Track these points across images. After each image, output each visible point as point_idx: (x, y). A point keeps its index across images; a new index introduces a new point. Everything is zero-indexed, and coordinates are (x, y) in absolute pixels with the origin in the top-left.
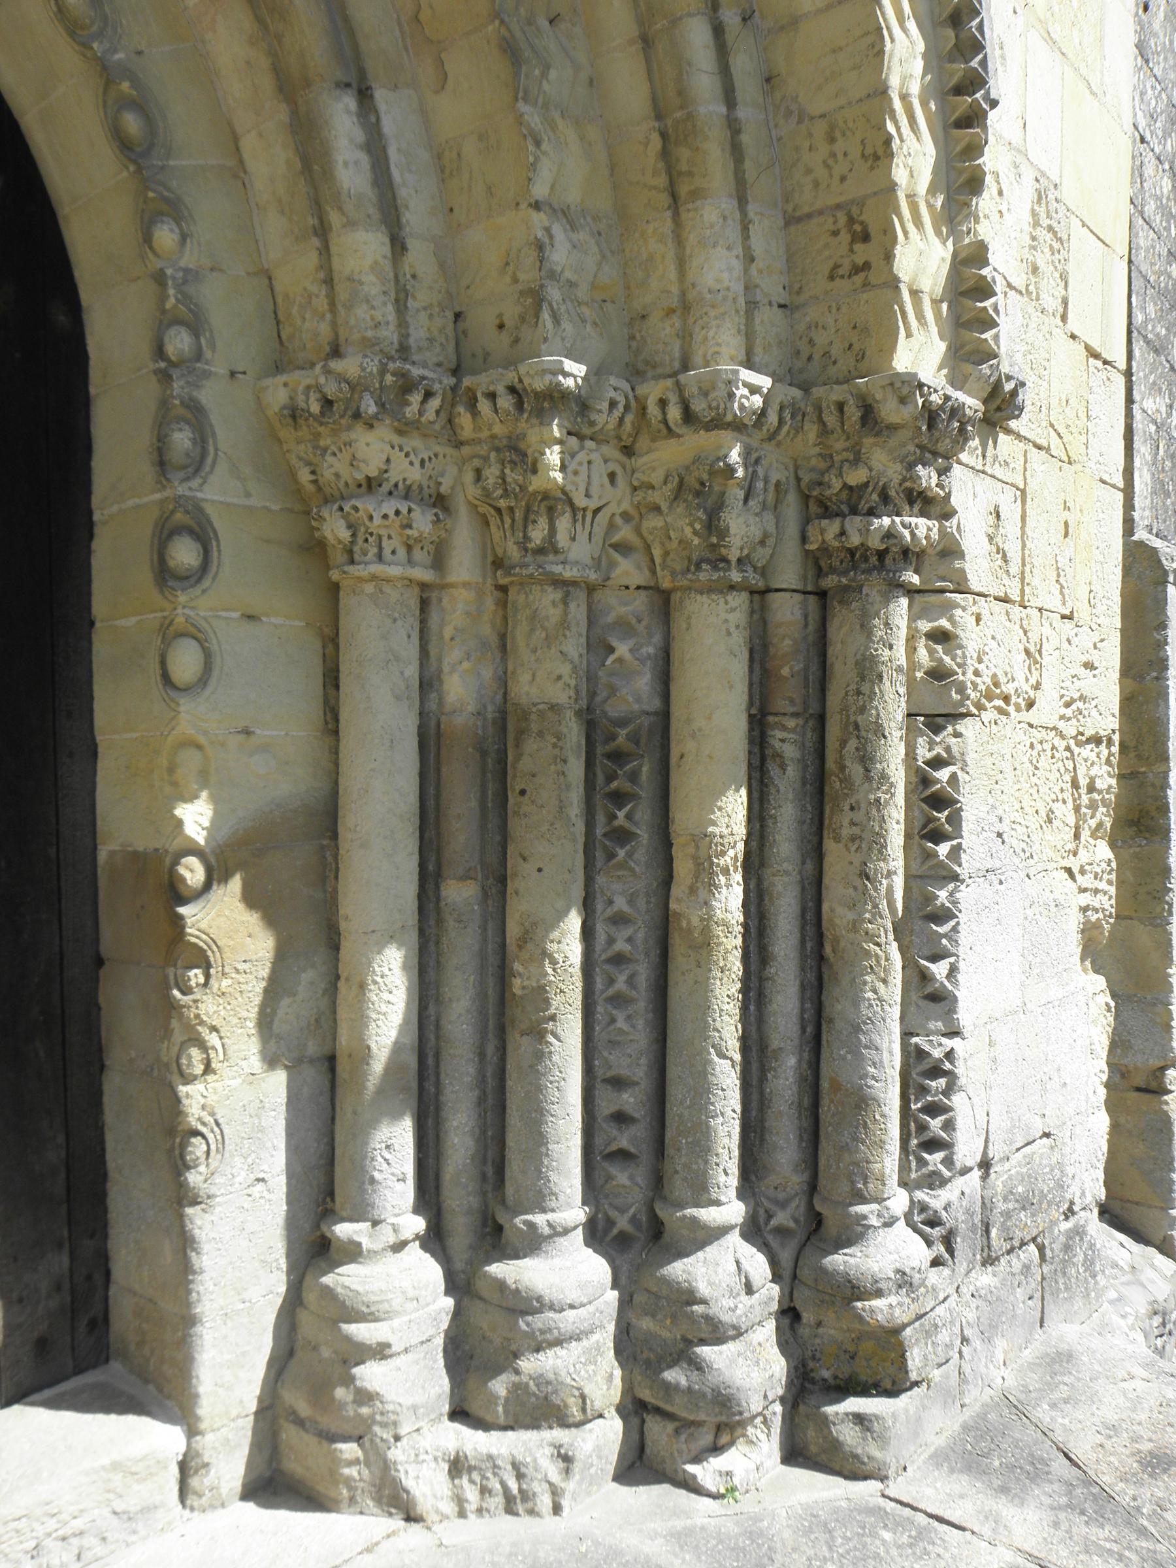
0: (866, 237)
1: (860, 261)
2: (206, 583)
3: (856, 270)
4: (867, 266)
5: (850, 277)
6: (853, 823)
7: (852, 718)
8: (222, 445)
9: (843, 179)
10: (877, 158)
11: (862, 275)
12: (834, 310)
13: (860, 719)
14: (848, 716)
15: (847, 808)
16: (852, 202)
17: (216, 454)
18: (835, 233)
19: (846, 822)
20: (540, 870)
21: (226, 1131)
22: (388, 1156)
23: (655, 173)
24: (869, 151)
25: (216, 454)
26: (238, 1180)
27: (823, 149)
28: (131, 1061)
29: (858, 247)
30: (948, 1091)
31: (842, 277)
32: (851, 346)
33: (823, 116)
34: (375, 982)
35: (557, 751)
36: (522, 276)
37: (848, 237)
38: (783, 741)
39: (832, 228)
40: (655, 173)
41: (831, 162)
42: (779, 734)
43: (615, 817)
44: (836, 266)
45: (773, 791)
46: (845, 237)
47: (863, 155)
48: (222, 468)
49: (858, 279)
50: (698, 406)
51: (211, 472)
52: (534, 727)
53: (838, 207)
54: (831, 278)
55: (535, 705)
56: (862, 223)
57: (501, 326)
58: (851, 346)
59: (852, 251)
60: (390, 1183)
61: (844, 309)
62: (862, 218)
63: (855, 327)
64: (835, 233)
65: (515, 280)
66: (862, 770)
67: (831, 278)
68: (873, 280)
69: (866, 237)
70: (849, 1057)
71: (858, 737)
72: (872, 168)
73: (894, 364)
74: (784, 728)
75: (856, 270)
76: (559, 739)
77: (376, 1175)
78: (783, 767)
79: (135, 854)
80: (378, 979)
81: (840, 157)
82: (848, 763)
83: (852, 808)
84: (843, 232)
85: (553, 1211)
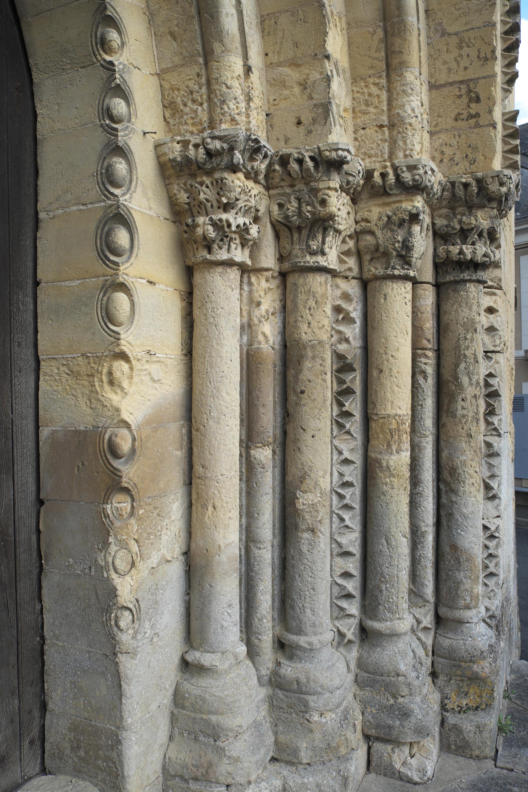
0: (478, 100)
1: (473, 112)
2: (132, 260)
3: (471, 116)
4: (477, 115)
5: (467, 120)
6: (463, 408)
7: (462, 352)
8: (139, 175)
9: (466, 68)
10: (486, 59)
11: (474, 120)
12: (457, 137)
13: (466, 352)
14: (460, 351)
15: (460, 400)
16: (471, 80)
17: (137, 181)
18: (460, 97)
19: (459, 407)
20: (313, 437)
21: (141, 605)
22: (230, 611)
23: (378, 50)
24: (482, 55)
25: (137, 181)
26: (147, 635)
27: (455, 53)
28: (69, 566)
29: (473, 105)
30: (497, 546)
31: (463, 119)
32: (467, 156)
33: (456, 34)
34: (222, 506)
35: (322, 368)
36: (315, 96)
37: (467, 100)
38: (425, 364)
39: (458, 94)
40: (378, 50)
41: (459, 59)
42: (424, 360)
43: (344, 405)
44: (459, 114)
45: (420, 390)
46: (465, 100)
47: (478, 57)
48: (139, 189)
49: (472, 121)
50: (407, 176)
51: (134, 192)
52: (310, 354)
53: (461, 82)
54: (456, 120)
55: (310, 341)
56: (476, 92)
57: (299, 123)
58: (467, 156)
59: (469, 106)
60: (231, 628)
61: (463, 136)
62: (475, 90)
63: (470, 146)
64: (460, 97)
65: (311, 98)
66: (468, 380)
67: (456, 120)
68: (481, 122)
69: (478, 100)
70: (462, 533)
71: (466, 362)
72: (483, 65)
73: (493, 166)
74: (426, 357)
75: (471, 116)
76: (323, 361)
77: (224, 623)
78: (425, 378)
79: (77, 432)
80: (225, 505)
81: (465, 57)
82: (460, 376)
83: (463, 400)
84: (464, 97)
85: (321, 634)
